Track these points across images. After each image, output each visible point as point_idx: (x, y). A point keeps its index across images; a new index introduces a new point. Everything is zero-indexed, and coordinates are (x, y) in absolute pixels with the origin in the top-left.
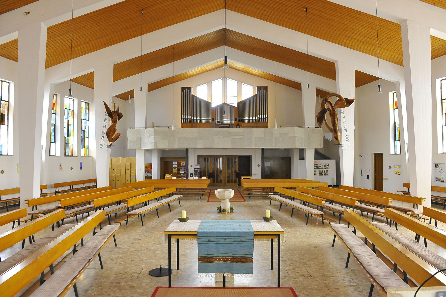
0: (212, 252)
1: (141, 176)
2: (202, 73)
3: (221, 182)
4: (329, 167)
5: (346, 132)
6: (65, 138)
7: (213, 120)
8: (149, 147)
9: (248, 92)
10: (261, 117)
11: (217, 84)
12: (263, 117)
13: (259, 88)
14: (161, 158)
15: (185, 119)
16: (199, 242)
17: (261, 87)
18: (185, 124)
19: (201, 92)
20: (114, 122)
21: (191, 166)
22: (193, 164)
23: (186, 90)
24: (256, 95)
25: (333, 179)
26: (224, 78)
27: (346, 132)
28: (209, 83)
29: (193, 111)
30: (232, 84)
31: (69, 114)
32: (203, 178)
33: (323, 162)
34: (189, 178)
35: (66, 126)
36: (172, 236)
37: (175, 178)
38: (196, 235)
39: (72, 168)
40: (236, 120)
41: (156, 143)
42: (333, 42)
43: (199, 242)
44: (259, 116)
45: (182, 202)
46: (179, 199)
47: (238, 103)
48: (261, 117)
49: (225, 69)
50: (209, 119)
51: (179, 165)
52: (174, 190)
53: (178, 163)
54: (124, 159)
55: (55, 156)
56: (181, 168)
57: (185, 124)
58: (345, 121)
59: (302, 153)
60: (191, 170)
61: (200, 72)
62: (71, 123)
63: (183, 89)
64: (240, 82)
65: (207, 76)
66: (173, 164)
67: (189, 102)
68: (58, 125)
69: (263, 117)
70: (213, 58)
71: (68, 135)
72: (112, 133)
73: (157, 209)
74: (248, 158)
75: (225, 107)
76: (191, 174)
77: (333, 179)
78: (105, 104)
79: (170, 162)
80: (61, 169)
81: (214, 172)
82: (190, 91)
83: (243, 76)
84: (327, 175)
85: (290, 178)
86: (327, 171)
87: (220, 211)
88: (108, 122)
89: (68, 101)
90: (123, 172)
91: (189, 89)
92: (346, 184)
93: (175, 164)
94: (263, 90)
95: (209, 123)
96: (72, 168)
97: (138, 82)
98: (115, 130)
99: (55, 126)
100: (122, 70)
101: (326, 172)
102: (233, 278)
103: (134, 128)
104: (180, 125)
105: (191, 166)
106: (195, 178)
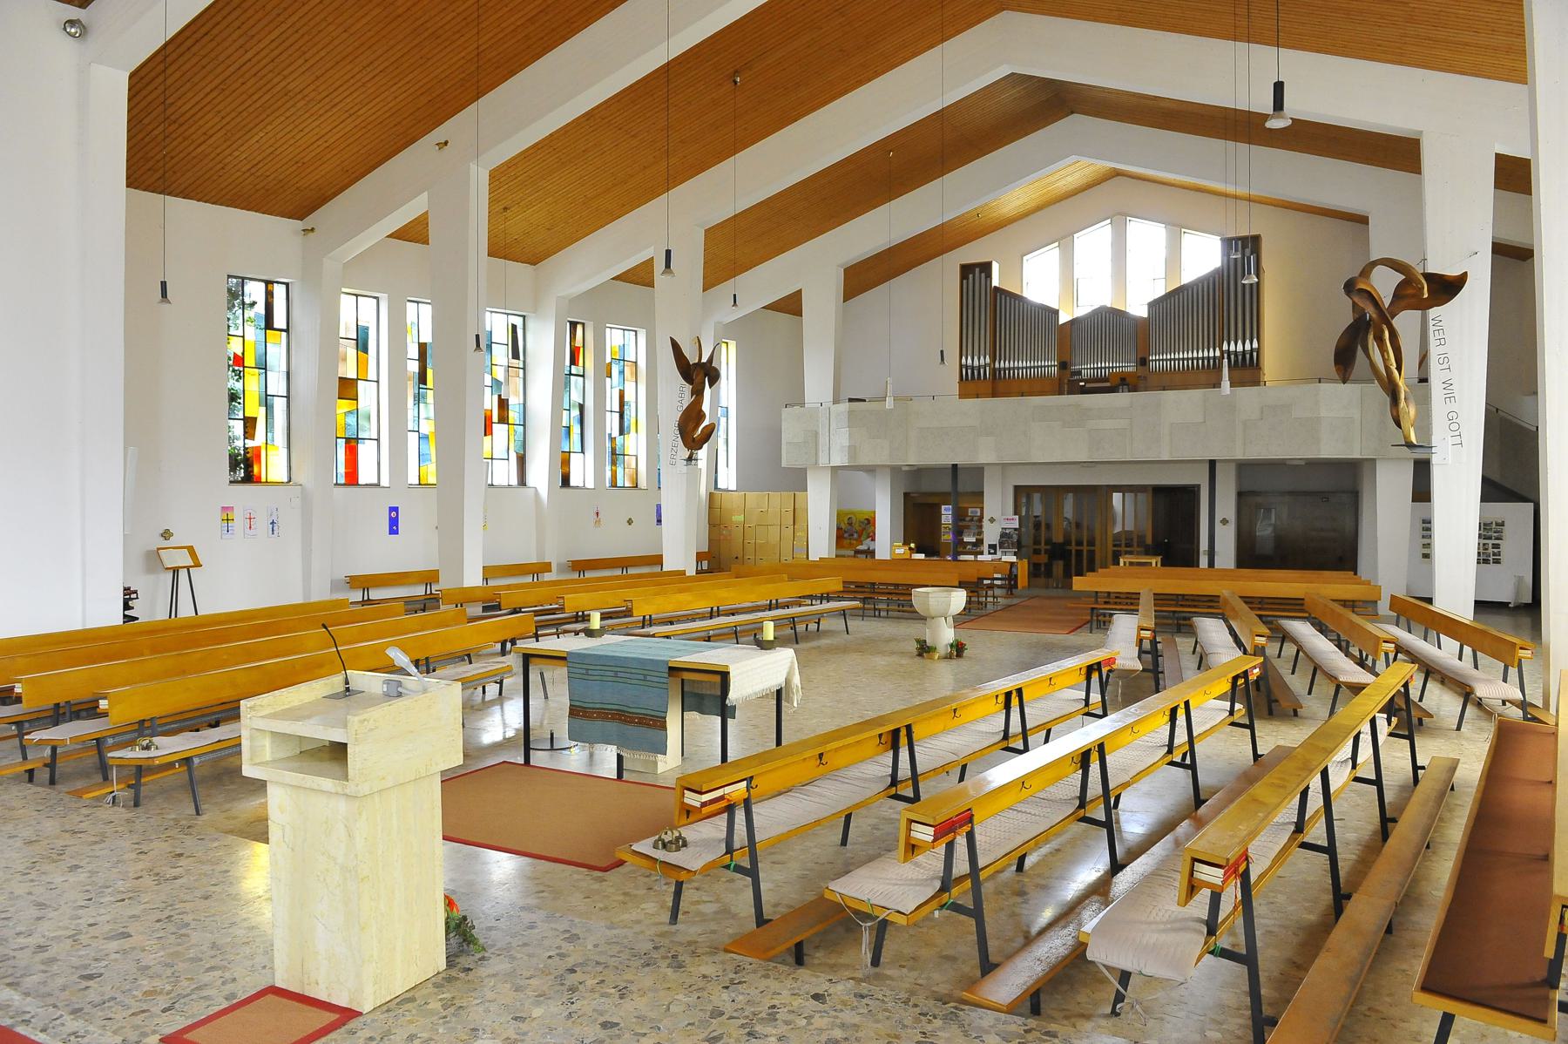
0: (602, 695)
1: (821, 543)
2: (1039, 208)
4: (1507, 530)
5: (1450, 397)
6: (612, 440)
7: (1063, 366)
8: (839, 459)
9: (1203, 256)
10: (1232, 348)
11: (1093, 242)
12: (1240, 348)
13: (1228, 243)
15: (973, 368)
18: (974, 384)
19: (1039, 279)
20: (698, 393)
21: (992, 520)
22: (998, 514)
23: (974, 273)
25: (1520, 580)
26: (1119, 218)
27: (1450, 397)
28: (1065, 239)
29: (1006, 343)
30: (1146, 236)
31: (622, 372)
32: (963, 557)
33: (1502, 510)
35: (616, 407)
36: (533, 660)
37: (922, 556)
38: (564, 659)
39: (630, 522)
40: (1143, 362)
41: (853, 450)
42: (1401, 63)
44: (1225, 347)
45: (854, 624)
46: (843, 613)
48: (1232, 348)
49: (1112, 194)
50: (1050, 366)
51: (959, 515)
54: (776, 497)
55: (584, 488)
56: (968, 527)
57: (974, 384)
58: (1445, 358)
60: (991, 534)
61: (1033, 204)
62: (629, 397)
63: (966, 270)
64: (1176, 227)
65: (1057, 217)
67: (991, 312)
68: (589, 405)
69: (1240, 348)
70: (1063, 159)
71: (622, 432)
72: (691, 425)
75: (1109, 322)
76: (993, 547)
77: (1520, 580)
78: (675, 346)
79: (934, 508)
80: (598, 522)
81: (1067, 542)
82: (989, 276)
83: (1180, 205)
84: (1497, 562)
85: (1354, 569)
86: (1496, 546)
87: (924, 649)
88: (676, 394)
89: (615, 337)
90: (773, 534)
91: (986, 268)
94: (1246, 248)
95: (1049, 378)
96: (630, 522)
97: (815, 266)
98: (701, 416)
99: (582, 407)
100: (736, 247)
101: (1491, 550)
102: (655, 763)
103: (802, 404)
104: (955, 387)
105: (992, 520)
106: (1004, 558)
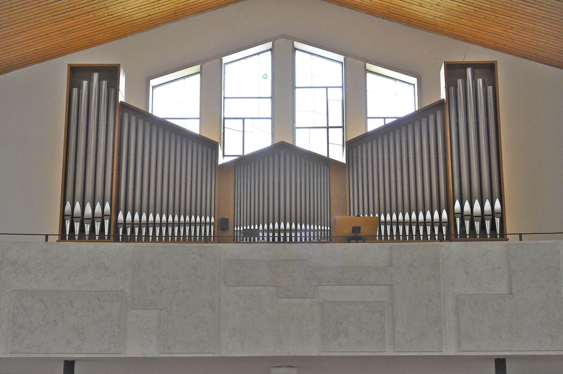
17: (463, 66)
47: (351, 146)
91: (110, 73)
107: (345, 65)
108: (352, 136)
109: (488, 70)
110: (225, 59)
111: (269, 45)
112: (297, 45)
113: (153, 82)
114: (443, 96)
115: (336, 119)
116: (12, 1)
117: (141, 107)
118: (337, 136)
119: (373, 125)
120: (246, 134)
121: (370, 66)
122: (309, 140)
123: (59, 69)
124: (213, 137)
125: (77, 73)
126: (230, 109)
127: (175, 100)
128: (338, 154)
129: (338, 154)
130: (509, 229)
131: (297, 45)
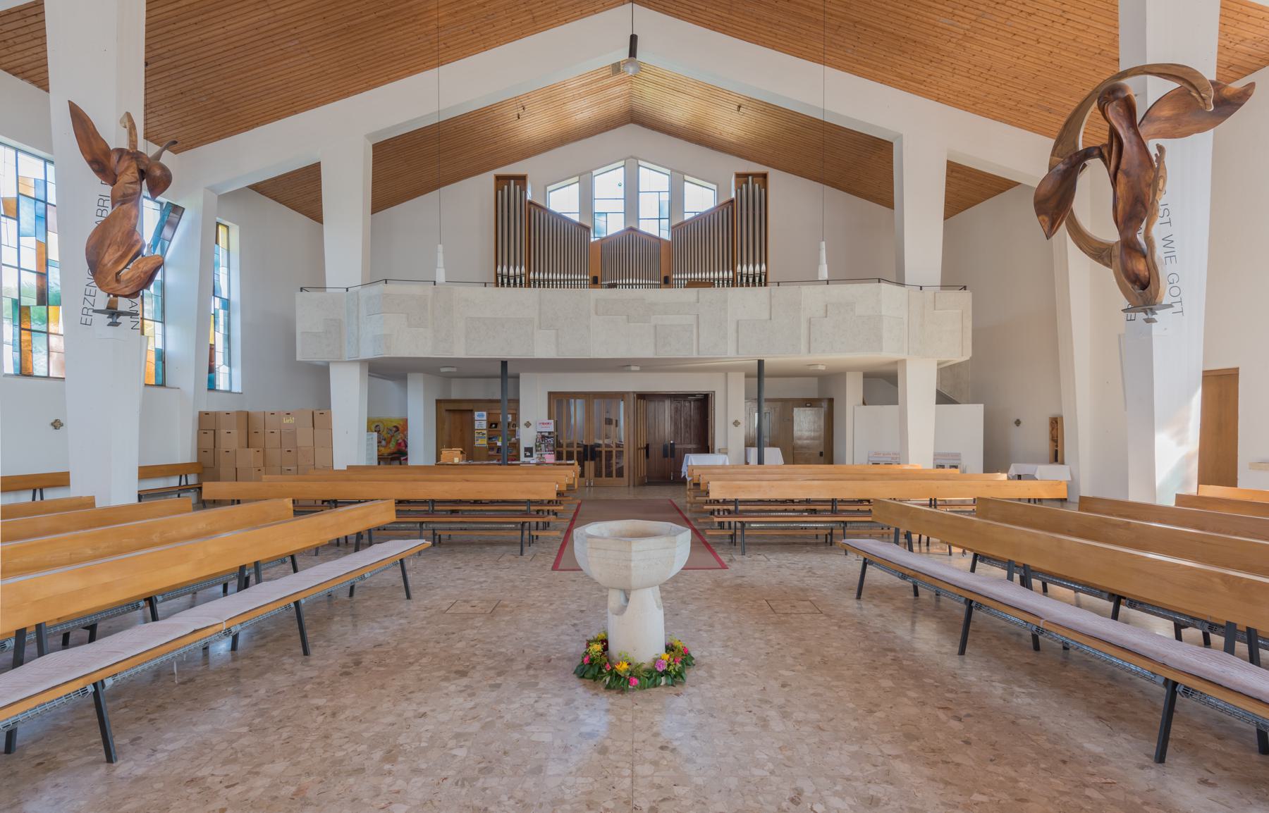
3: (620, 473)
14: (438, 401)
16: (1112, 22)
17: (747, 175)
23: (510, 185)
24: (732, 201)
34: (523, 458)
43: (1112, 22)
47: (674, 229)
52: (383, 514)
53: (489, 415)
59: (883, 384)
60: (527, 437)
66: (473, 421)
73: (401, 560)
74: (703, 402)
76: (529, 450)
82: (524, 188)
91: (521, 180)
92: (222, 388)
93: (481, 420)
107: (671, 177)
108: (674, 224)
109: (765, 176)
110: (595, 173)
111: (622, 163)
112: (640, 162)
113: (549, 188)
114: (733, 196)
115: (665, 213)
116: (410, 3)
117: (542, 204)
118: (665, 223)
119: (687, 217)
120: (611, 224)
121: (687, 177)
122: (234, 390)
123: (488, 179)
124: (588, 224)
125: (498, 178)
126: (598, 207)
127: (563, 201)
128: (666, 235)
129: (666, 235)
130: (769, 279)
131: (640, 162)
